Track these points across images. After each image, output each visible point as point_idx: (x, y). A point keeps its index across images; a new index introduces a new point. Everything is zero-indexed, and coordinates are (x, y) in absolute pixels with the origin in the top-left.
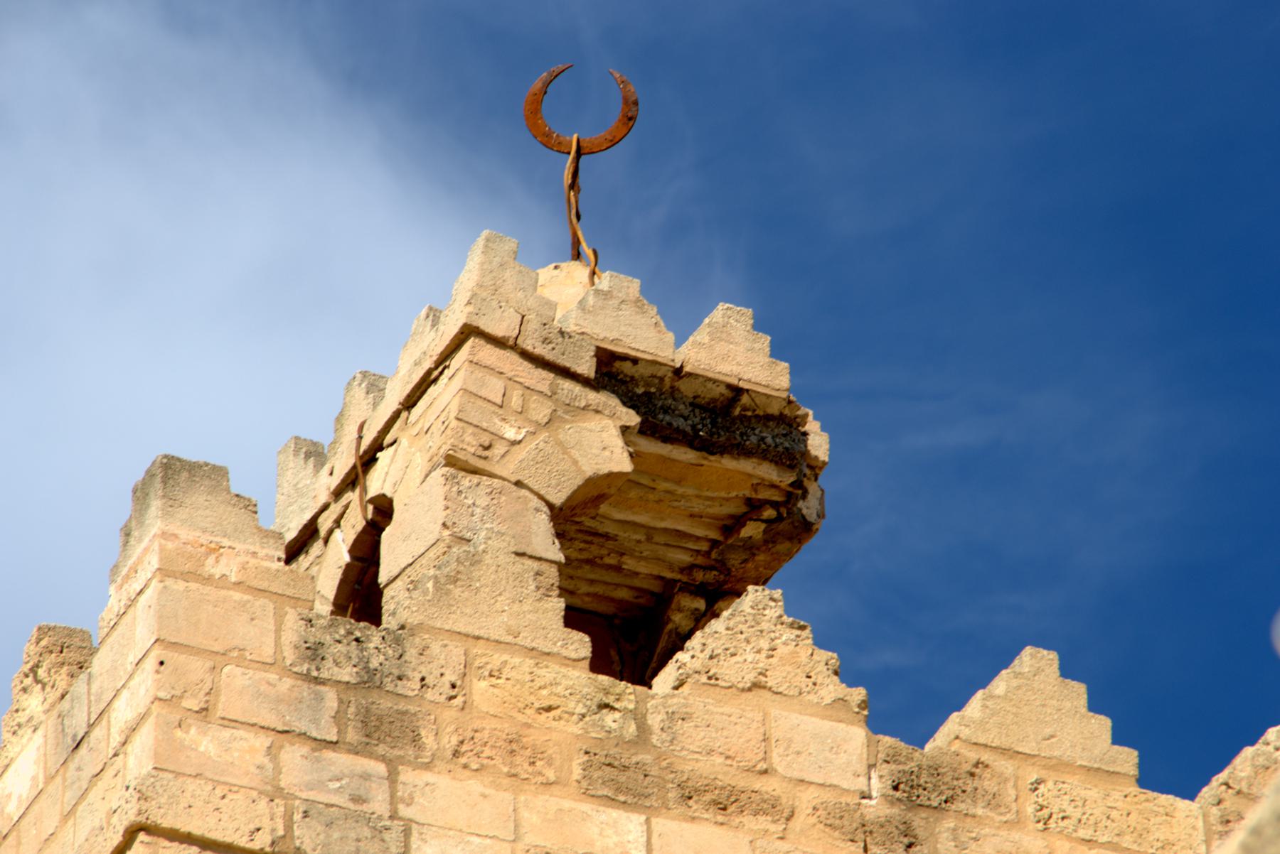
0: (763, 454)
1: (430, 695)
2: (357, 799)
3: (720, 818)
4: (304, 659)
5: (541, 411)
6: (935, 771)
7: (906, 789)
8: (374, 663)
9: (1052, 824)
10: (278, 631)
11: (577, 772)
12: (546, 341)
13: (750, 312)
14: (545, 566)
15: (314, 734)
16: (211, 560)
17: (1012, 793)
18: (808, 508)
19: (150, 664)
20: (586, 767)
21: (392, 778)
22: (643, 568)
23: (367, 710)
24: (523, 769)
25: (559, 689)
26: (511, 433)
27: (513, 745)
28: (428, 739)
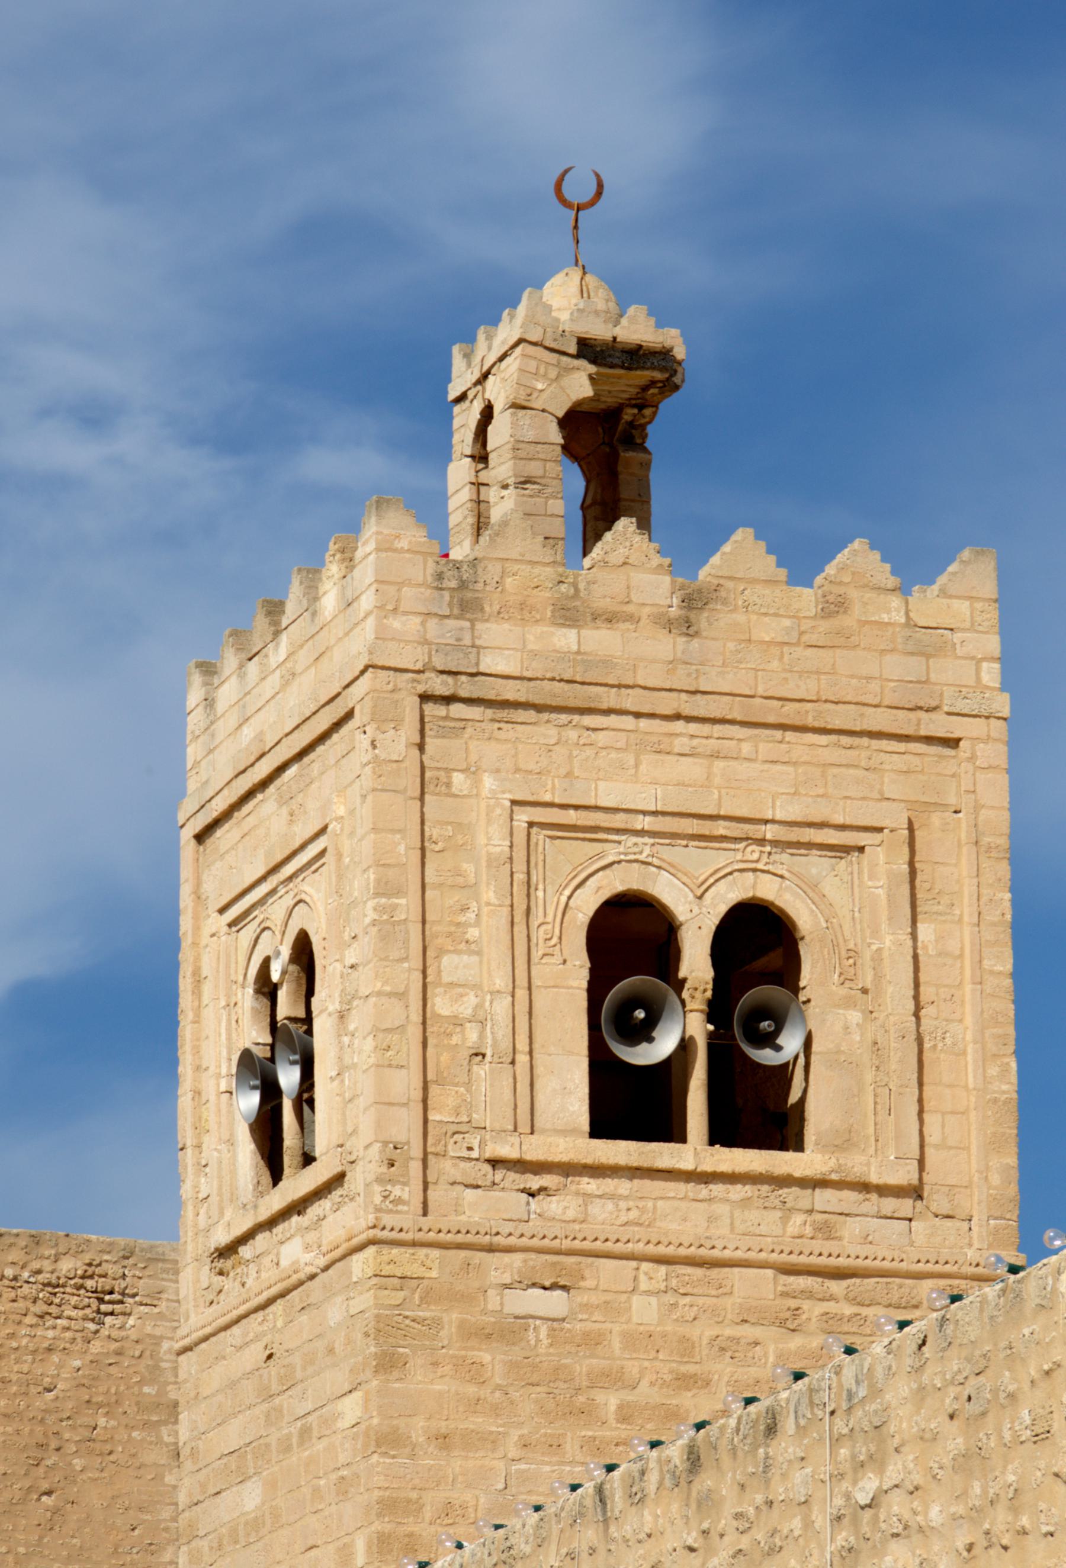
1: (488, 588)
2: (458, 640)
5: (553, 373)
6: (700, 591)
8: (465, 578)
11: (549, 614)
12: (555, 340)
13: (645, 307)
14: (555, 447)
15: (440, 613)
17: (733, 596)
18: (677, 380)
19: (373, 588)
20: (553, 612)
21: (472, 628)
22: (609, 400)
24: (527, 616)
25: (542, 578)
26: (540, 386)
28: (487, 609)
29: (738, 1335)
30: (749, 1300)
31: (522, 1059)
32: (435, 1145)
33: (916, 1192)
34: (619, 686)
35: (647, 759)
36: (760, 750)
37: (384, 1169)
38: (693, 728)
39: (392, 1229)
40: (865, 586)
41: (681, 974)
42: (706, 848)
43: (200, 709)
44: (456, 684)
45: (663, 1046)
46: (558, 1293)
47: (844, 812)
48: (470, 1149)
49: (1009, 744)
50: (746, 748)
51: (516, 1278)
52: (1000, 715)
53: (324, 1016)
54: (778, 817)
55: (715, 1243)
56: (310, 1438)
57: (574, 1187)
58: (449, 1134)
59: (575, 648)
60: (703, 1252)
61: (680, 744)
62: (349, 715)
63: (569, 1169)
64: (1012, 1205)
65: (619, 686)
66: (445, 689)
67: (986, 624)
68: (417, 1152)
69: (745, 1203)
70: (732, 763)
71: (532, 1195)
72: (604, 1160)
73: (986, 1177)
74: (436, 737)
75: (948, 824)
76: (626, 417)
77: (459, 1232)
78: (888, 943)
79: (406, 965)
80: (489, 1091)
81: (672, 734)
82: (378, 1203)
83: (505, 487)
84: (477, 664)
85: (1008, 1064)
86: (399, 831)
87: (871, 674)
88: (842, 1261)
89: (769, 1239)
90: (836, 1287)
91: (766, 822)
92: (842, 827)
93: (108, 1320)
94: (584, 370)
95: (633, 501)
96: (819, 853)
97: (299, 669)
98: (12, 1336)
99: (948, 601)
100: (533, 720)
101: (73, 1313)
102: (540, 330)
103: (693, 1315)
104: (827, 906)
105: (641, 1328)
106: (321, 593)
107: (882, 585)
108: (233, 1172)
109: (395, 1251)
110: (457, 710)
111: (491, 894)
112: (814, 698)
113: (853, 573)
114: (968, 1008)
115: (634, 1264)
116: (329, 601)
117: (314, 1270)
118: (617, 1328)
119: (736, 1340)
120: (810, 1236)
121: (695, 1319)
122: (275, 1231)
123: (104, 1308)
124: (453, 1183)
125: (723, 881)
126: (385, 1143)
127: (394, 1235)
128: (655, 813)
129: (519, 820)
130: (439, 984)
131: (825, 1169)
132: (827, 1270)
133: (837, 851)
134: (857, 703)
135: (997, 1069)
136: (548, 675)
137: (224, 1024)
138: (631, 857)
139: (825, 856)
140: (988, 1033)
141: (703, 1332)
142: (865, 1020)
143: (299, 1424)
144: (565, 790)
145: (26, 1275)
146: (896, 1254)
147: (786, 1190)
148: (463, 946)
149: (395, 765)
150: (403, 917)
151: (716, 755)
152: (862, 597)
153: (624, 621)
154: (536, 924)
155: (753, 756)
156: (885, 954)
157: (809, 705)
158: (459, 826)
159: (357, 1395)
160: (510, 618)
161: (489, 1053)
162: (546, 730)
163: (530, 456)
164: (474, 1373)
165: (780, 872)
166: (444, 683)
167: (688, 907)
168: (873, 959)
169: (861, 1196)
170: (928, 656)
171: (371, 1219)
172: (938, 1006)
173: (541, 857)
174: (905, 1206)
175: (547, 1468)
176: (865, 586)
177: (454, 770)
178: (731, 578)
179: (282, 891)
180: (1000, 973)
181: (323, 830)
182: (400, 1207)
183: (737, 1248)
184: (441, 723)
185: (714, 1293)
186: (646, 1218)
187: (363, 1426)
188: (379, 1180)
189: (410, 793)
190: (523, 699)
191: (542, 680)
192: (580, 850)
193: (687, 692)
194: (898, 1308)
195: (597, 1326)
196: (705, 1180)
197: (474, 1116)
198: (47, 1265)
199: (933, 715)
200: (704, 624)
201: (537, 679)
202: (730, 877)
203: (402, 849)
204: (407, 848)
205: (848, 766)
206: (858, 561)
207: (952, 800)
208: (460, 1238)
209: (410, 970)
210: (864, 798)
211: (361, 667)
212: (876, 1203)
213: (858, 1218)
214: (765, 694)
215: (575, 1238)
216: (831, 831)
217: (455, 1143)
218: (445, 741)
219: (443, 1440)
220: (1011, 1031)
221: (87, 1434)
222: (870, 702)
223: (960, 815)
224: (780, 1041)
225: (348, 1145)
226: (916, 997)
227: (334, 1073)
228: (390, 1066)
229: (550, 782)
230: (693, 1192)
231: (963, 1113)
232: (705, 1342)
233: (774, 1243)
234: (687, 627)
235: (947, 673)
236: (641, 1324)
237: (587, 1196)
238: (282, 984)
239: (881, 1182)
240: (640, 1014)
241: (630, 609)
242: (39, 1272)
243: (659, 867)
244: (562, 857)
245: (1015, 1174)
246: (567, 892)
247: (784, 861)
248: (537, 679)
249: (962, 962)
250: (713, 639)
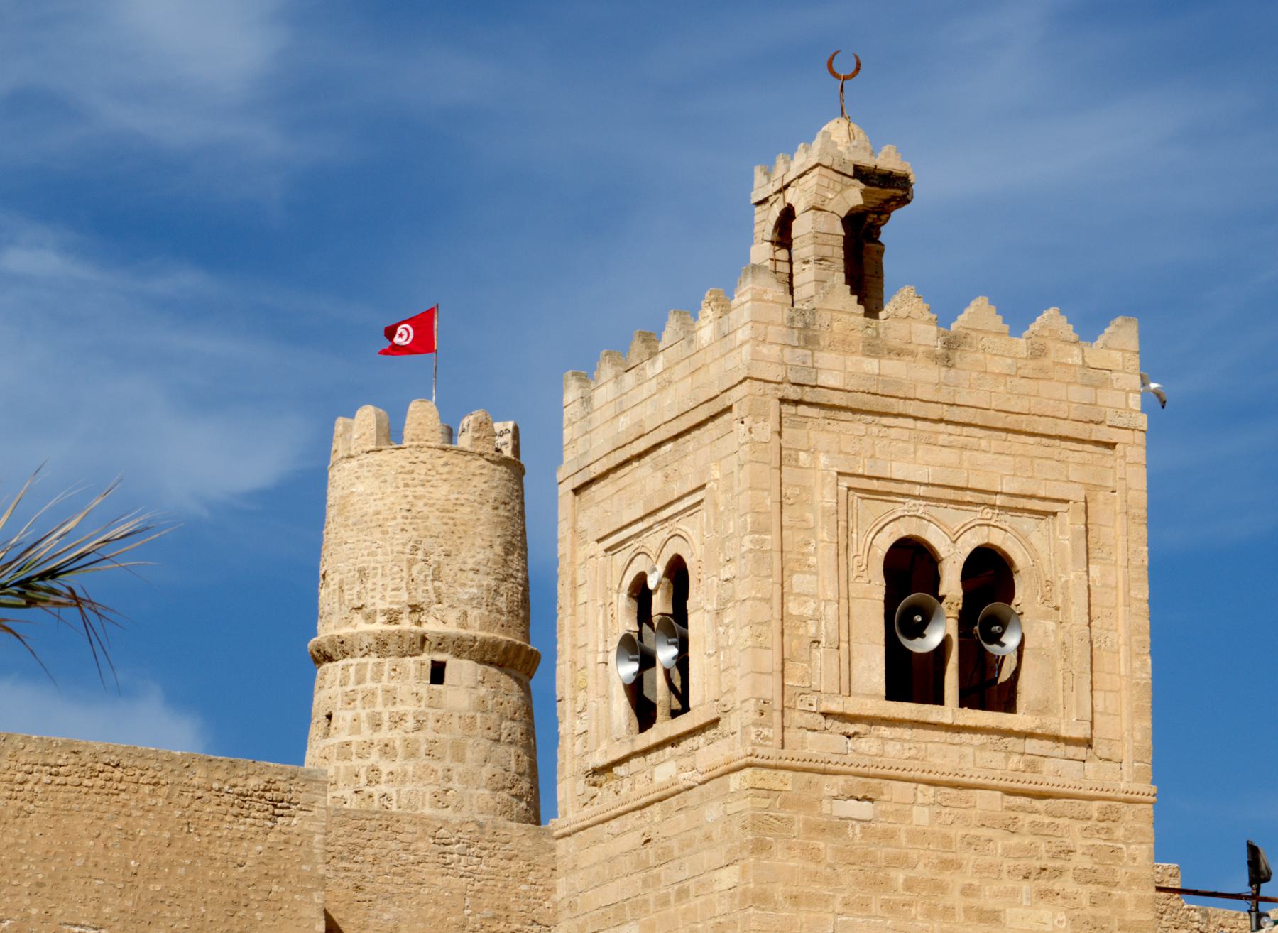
0: (898, 188)
5: (838, 188)
6: (955, 337)
19: (749, 325)
21: (813, 355)
26: (830, 196)
27: (844, 342)
31: (844, 645)
33: (1088, 743)
34: (905, 399)
35: (922, 448)
37: (757, 716)
38: (951, 428)
41: (941, 593)
43: (577, 404)
45: (933, 639)
46: (866, 803)
49: (1147, 448)
50: (984, 443)
53: (699, 613)
56: (688, 897)
57: (875, 733)
60: (957, 778)
61: (943, 439)
62: (729, 409)
63: (873, 721)
65: (905, 399)
68: (778, 706)
69: (982, 747)
70: (975, 453)
71: (849, 737)
72: (896, 715)
80: (823, 666)
83: (807, 262)
87: (1061, 398)
88: (1044, 788)
90: (1039, 804)
91: (997, 493)
92: (1044, 499)
93: (280, 820)
97: (675, 378)
98: (217, 828)
101: (257, 815)
104: (1032, 549)
106: (697, 327)
108: (609, 716)
109: (764, 772)
110: (803, 409)
111: (825, 534)
114: (1121, 622)
115: (914, 785)
116: (706, 331)
117: (692, 784)
118: (903, 828)
119: (978, 838)
122: (648, 757)
123: (277, 811)
126: (758, 699)
127: (764, 761)
128: (927, 485)
130: (791, 593)
131: (1033, 726)
137: (601, 617)
141: (957, 832)
143: (676, 887)
145: (226, 788)
146: (1077, 784)
148: (806, 569)
151: (964, 448)
156: (1070, 584)
158: (803, 488)
159: (735, 868)
161: (823, 641)
162: (858, 426)
164: (813, 855)
166: (795, 391)
169: (1054, 745)
170: (1096, 388)
171: (749, 750)
174: (1081, 752)
175: (860, 920)
178: (974, 330)
179: (657, 528)
181: (703, 487)
186: (920, 755)
187: (740, 889)
188: (755, 724)
190: (844, 405)
192: (878, 508)
198: (240, 782)
199: (1100, 427)
200: (957, 359)
203: (768, 502)
204: (772, 502)
205: (1047, 458)
206: (1051, 321)
207: (1110, 484)
208: (805, 765)
209: (774, 583)
211: (741, 378)
216: (1037, 501)
219: (795, 899)
220: (1148, 638)
221: (265, 895)
224: (1003, 640)
225: (723, 700)
226: (1089, 614)
227: (711, 652)
230: (949, 738)
234: (946, 360)
235: (1108, 399)
237: (884, 739)
238: (656, 590)
239: (1067, 735)
240: (918, 618)
241: (911, 347)
242: (235, 786)
245: (1150, 733)
246: (871, 535)
247: (1007, 520)
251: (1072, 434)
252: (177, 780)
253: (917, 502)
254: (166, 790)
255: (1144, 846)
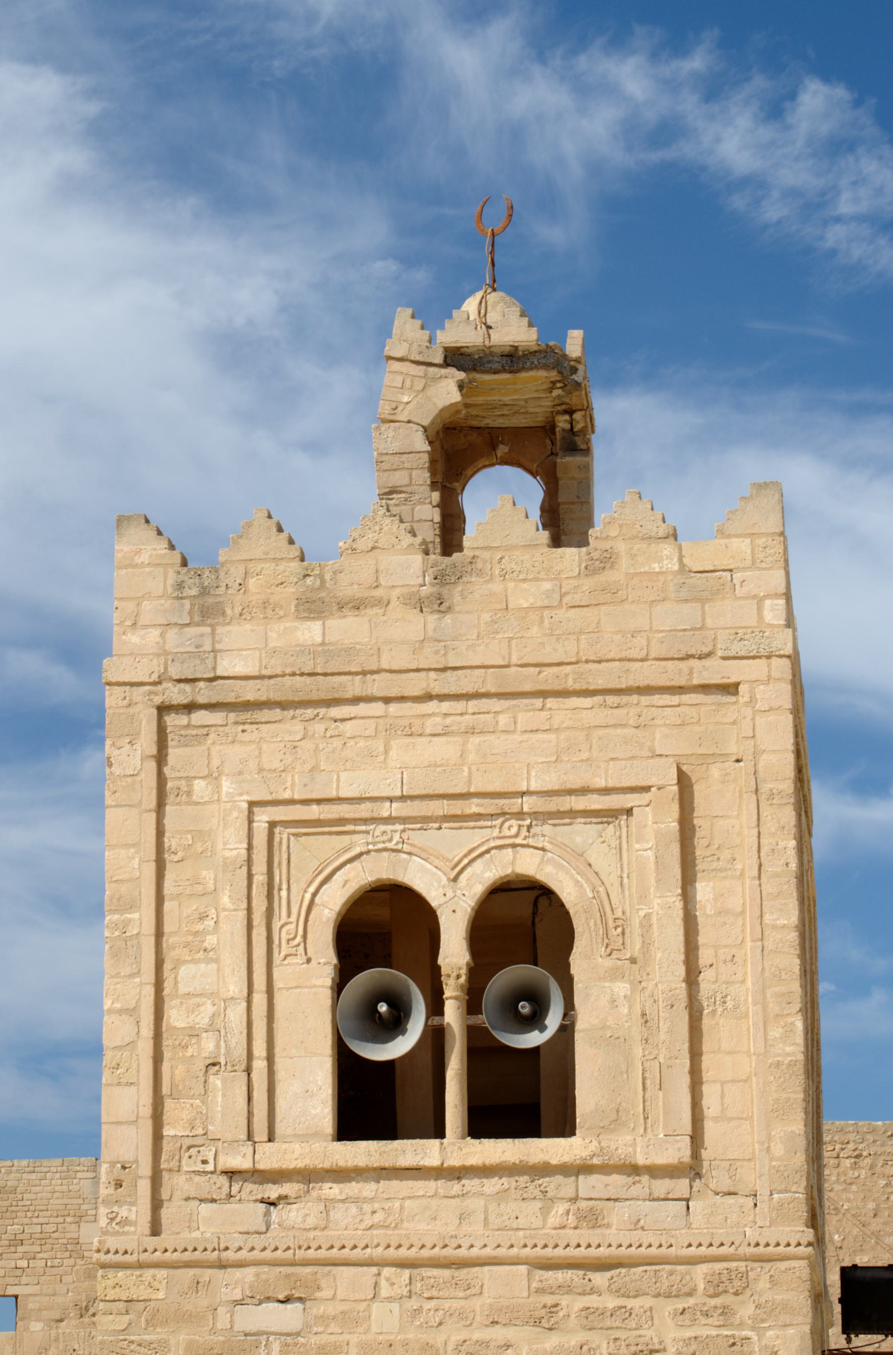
1: (230, 591)
3: (356, 613)
4: (175, 590)
5: (419, 385)
7: (440, 578)
8: (206, 584)
9: (507, 576)
10: (165, 580)
11: (293, 608)
12: (420, 353)
15: (180, 622)
16: (137, 557)
17: (489, 566)
20: (297, 606)
23: (203, 605)
25: (287, 574)
26: (406, 399)
27: (266, 603)
28: (229, 612)
29: (488, 1338)
30: (501, 1300)
31: (260, 1065)
32: (167, 1161)
34: (364, 673)
36: (519, 721)
38: (446, 706)
39: (117, 1252)
40: (634, 537)
42: (461, 828)
44: (194, 691)
47: (606, 773)
48: (204, 1162)
51: (248, 1293)
52: (782, 652)
54: (533, 788)
55: (461, 1242)
58: (184, 1148)
59: (319, 639)
61: (431, 725)
63: (309, 1176)
64: (798, 1176)
65: (364, 673)
66: (182, 698)
67: (770, 559)
68: (145, 1169)
70: (491, 737)
73: (769, 1148)
74: (177, 747)
75: (728, 774)
76: (561, 425)
77: (186, 1250)
78: (656, 907)
79: (137, 980)
81: (424, 715)
82: (104, 1225)
84: (214, 669)
85: (792, 1024)
86: (134, 845)
89: (521, 1233)
90: (599, 1279)
91: (523, 794)
92: (606, 791)
94: (453, 377)
95: (572, 503)
96: (583, 820)
99: (726, 541)
100: (277, 718)
102: (405, 346)
103: (437, 1320)
105: (381, 1338)
107: (653, 534)
110: (200, 717)
112: (574, 660)
113: (621, 526)
115: (374, 1270)
118: (354, 1339)
120: (572, 1226)
121: (440, 1324)
124: (187, 1199)
125: (479, 861)
127: (119, 1258)
128: (403, 798)
129: (259, 821)
132: (587, 1261)
133: (604, 816)
134: (620, 660)
135: (780, 1030)
136: (288, 671)
138: (381, 846)
139: (591, 823)
140: (769, 993)
142: (633, 991)
144: (306, 785)
147: (547, 1179)
148: (201, 955)
149: (130, 780)
150: (135, 932)
151: (471, 731)
152: (632, 548)
153: (372, 607)
154: (279, 924)
155: (512, 728)
156: (654, 919)
157: (569, 667)
160: (252, 618)
162: (291, 727)
163: (394, 467)
165: (540, 845)
167: (441, 891)
168: (641, 925)
169: (630, 1180)
170: (703, 601)
172: (717, 968)
173: (285, 856)
174: (681, 1186)
176: (634, 537)
177: (195, 778)
180: (784, 926)
182: (127, 1229)
183: (485, 1246)
184: (183, 732)
185: (461, 1294)
189: (144, 806)
191: (283, 676)
192: (327, 846)
193: (435, 670)
194: (669, 1297)
195: (333, 1338)
196: (457, 1174)
197: (210, 1127)
199: (706, 662)
200: (457, 598)
201: (276, 676)
202: (487, 856)
203: (136, 863)
205: (615, 726)
207: (733, 748)
209: (141, 984)
210: (633, 758)
212: (647, 1185)
213: (628, 1203)
214: (519, 663)
215: (309, 1248)
216: (595, 796)
217: (190, 1157)
218: (186, 749)
222: (636, 656)
223: (741, 764)
228: (119, 1084)
229: (289, 779)
230: (453, 1188)
231: (745, 1081)
232: (450, 1347)
233: (526, 1237)
235: (725, 615)
236: (381, 1333)
237: (328, 1203)
239: (648, 1162)
240: (383, 1008)
243: (410, 854)
244: (307, 854)
246: (312, 889)
248: (276, 676)
249: (744, 919)
250: (467, 612)
251: (663, 682)
252: (880, 1150)
253: (389, 828)
254: (868, 1161)
255: (791, 1331)
